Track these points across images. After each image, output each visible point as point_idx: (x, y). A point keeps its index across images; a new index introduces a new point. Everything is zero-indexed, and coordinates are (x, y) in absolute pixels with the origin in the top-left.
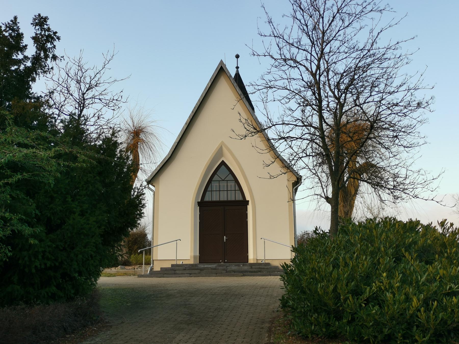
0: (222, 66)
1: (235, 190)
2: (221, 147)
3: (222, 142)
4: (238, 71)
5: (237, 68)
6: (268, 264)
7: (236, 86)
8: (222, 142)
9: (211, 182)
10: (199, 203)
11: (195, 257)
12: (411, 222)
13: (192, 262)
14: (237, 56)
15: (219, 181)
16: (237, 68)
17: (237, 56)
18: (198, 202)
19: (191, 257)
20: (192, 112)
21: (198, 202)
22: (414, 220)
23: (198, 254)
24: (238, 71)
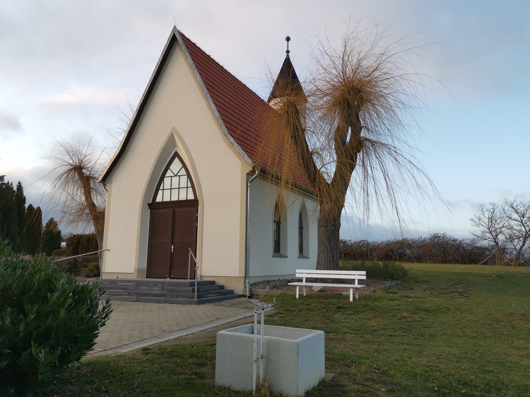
0: (174, 33)
1: (187, 187)
2: (172, 134)
3: (174, 128)
4: (288, 56)
5: (288, 52)
6: (213, 283)
7: (188, 56)
8: (174, 128)
9: (163, 180)
10: (149, 205)
11: (139, 271)
12: (29, 205)
13: (134, 277)
14: (288, 39)
15: (171, 177)
16: (288, 52)
17: (288, 39)
18: (149, 204)
19: (135, 270)
20: (143, 95)
21: (149, 204)
22: (148, 208)
23: (145, 266)
24: (288, 56)
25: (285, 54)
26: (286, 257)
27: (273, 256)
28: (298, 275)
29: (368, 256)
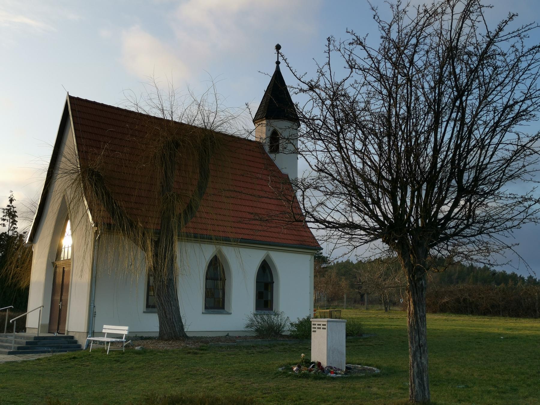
11: (42, 326)
14: (278, 47)
23: (47, 322)
25: (275, 65)
26: (230, 314)
27: (144, 312)
28: (104, 331)
29: (536, 311)
